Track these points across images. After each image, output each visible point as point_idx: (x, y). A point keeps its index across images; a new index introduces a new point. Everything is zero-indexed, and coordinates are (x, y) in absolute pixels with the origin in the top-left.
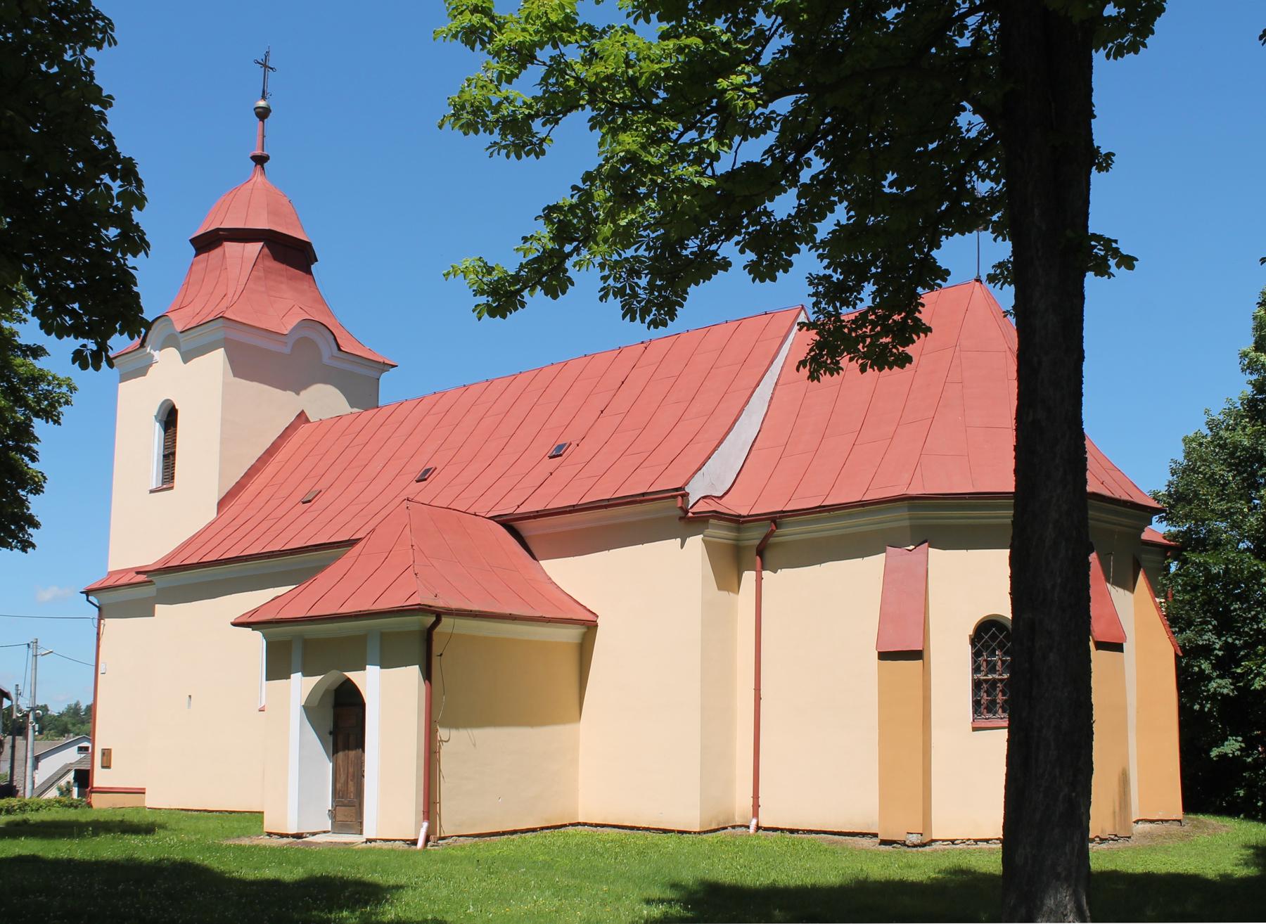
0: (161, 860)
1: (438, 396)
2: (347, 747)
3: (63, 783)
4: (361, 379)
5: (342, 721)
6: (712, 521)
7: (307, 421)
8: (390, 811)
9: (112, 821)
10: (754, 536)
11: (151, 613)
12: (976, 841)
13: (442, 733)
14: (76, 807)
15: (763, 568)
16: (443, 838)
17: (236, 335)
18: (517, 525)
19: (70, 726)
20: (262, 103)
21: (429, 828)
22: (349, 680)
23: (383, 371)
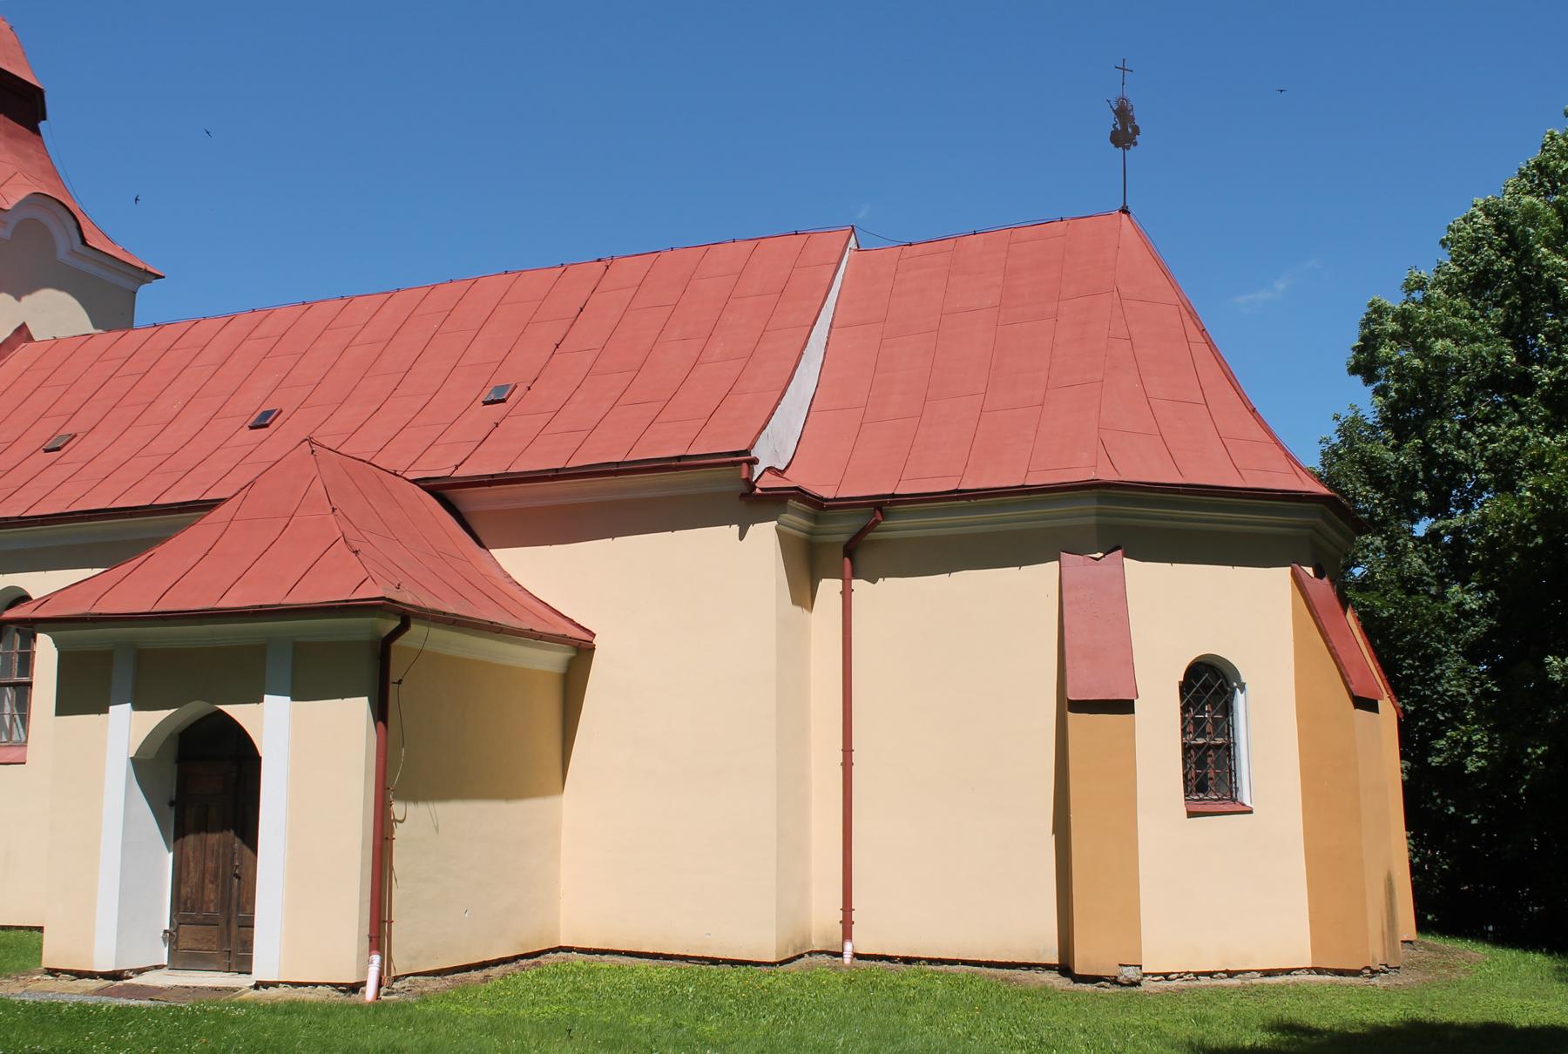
1: (261, 315)
4: (111, 289)
5: (206, 790)
6: (792, 503)
7: (30, 339)
10: (840, 530)
12: (1197, 975)
13: (398, 809)
15: (855, 575)
16: (396, 979)
18: (452, 494)
21: (382, 962)
23: (143, 282)
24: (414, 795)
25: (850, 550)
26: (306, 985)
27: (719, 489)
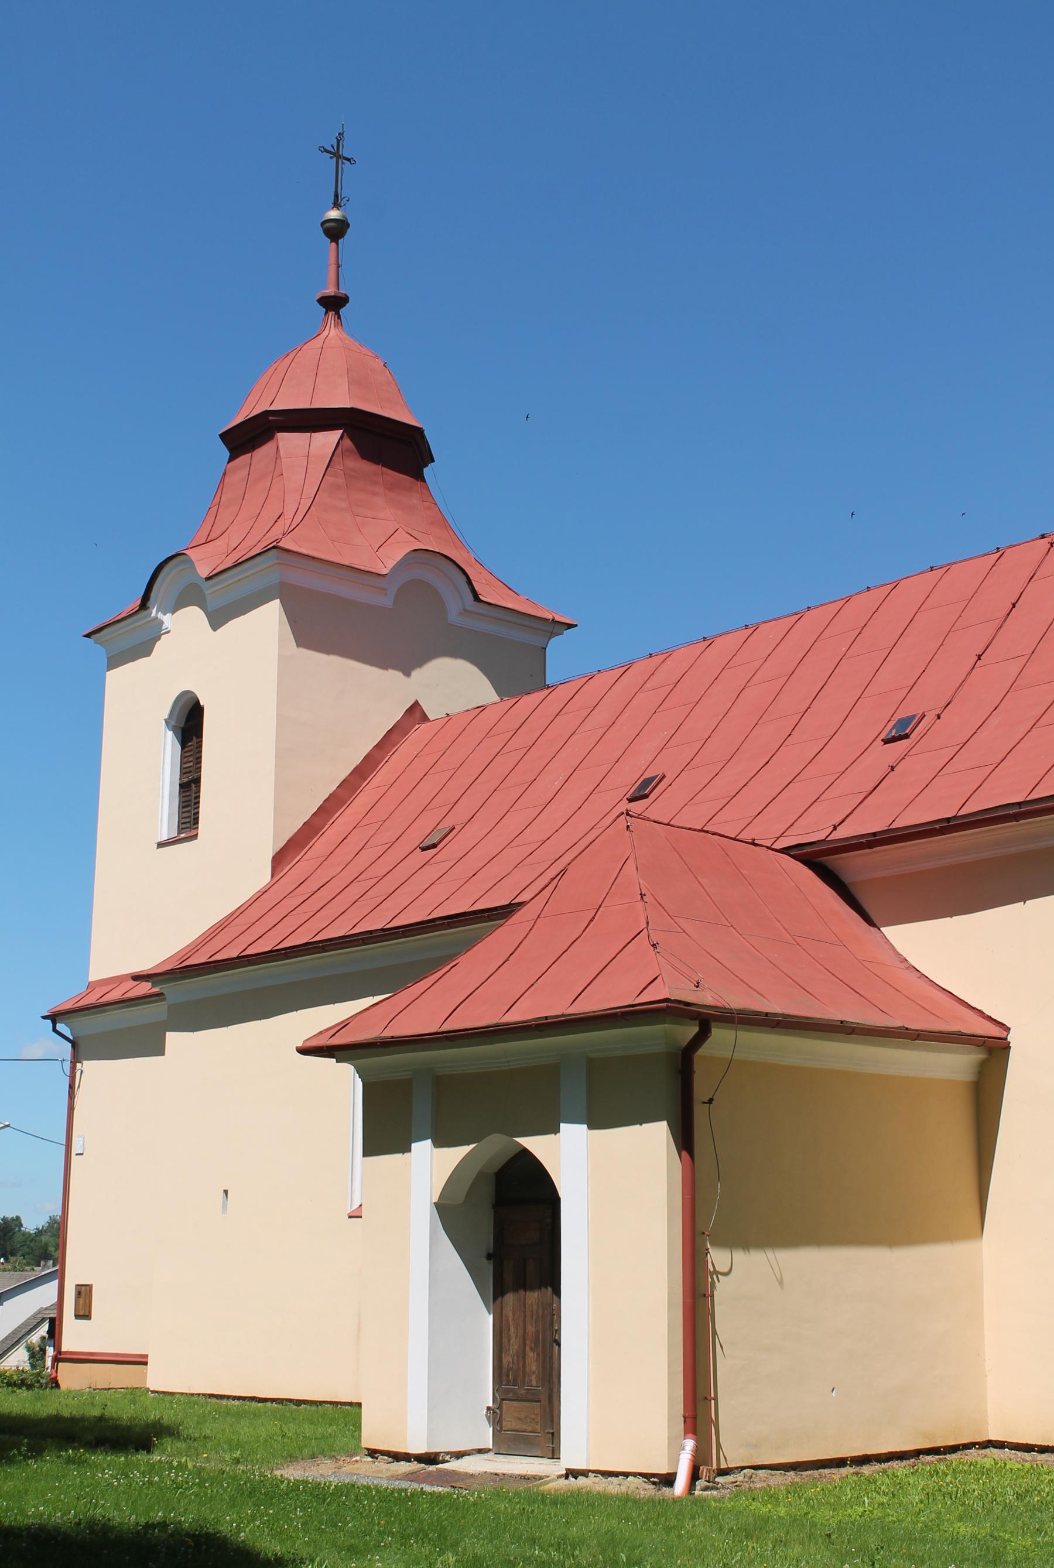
0: (148, 1526)
2: (522, 1284)
3: (35, 1338)
4: (515, 649)
5: (511, 1236)
7: (425, 718)
8: (614, 1414)
9: (82, 1419)
11: (159, 1049)
13: (718, 1258)
14: (30, 1387)
17: (300, 577)
18: (832, 861)
19: (51, 1249)
20: (334, 214)
22: (525, 1153)
23: (553, 634)
24: (744, 1238)
26: (616, 1474)
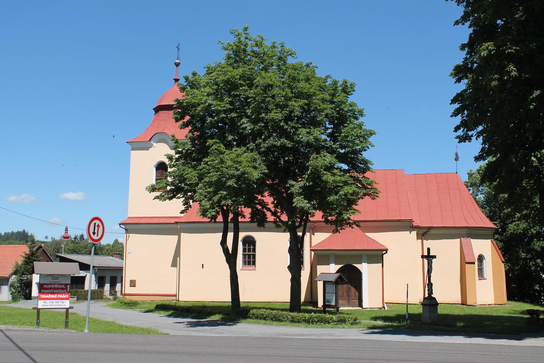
10: (422, 231)
25: (423, 235)
27: (406, 225)
